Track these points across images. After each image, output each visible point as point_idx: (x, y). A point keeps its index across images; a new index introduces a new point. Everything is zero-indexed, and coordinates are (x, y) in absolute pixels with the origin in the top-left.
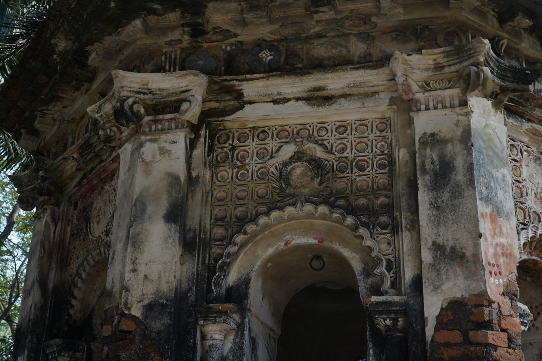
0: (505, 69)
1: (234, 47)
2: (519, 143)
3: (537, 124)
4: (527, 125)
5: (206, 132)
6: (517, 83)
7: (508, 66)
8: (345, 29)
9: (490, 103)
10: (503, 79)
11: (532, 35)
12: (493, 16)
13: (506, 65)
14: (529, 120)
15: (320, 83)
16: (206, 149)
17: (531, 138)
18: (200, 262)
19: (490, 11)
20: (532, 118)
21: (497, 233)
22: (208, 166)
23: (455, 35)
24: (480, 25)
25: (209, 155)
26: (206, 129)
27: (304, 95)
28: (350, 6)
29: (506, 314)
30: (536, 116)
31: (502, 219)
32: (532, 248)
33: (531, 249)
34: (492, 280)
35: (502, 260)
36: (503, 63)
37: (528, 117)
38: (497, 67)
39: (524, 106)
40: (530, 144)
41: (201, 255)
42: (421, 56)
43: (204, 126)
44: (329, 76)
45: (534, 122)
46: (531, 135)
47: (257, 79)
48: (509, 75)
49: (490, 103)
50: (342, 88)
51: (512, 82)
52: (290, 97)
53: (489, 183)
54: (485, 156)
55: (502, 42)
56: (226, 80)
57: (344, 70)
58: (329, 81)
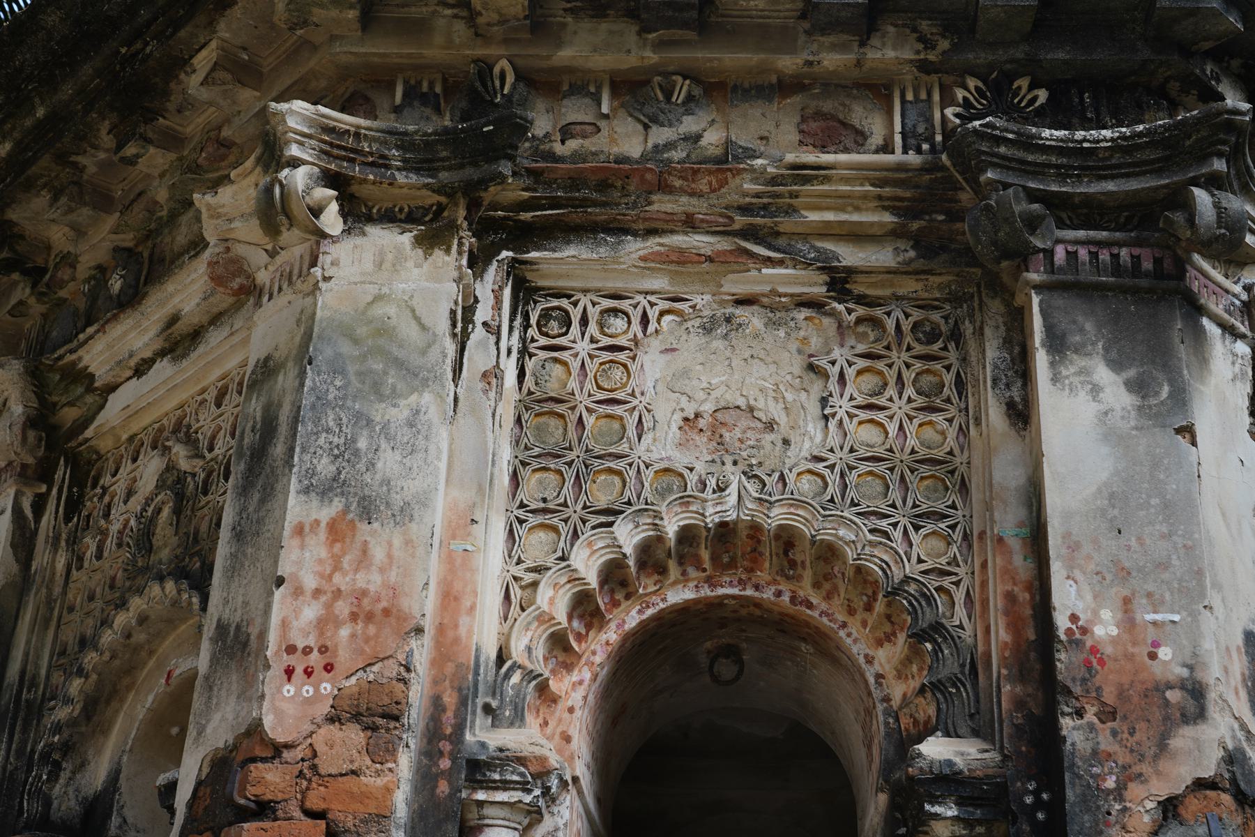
0: (427, 144)
1: (92, 282)
2: (639, 298)
3: (686, 233)
4: (634, 248)
5: (65, 473)
6: (475, 164)
7: (435, 133)
8: (207, 172)
9: (406, 239)
10: (429, 170)
11: (606, 16)
12: (455, 16)
13: (426, 134)
14: (652, 232)
15: (168, 310)
16: (61, 510)
17: (674, 275)
18: (12, 753)
19: (439, 9)
20: (659, 225)
21: (346, 566)
22: (63, 544)
23: (361, 101)
24: (409, 56)
25: (68, 519)
26: (66, 468)
27: (157, 346)
28: (199, 120)
29: (334, 772)
30: (663, 216)
31: (376, 525)
32: (707, 565)
33: (704, 570)
34: (289, 690)
35: (344, 632)
36: (416, 132)
37: (641, 226)
38: (398, 147)
39: (604, 205)
40: (678, 290)
41: (16, 737)
42: (234, 187)
43: (62, 462)
44: (170, 287)
45: (672, 232)
46: (673, 267)
47: (91, 337)
48: (444, 154)
49: (406, 239)
50: (198, 305)
51: (462, 166)
52: (148, 354)
53: (351, 442)
54: (353, 378)
55: (497, 70)
56: (61, 358)
57: (181, 267)
58: (176, 300)
